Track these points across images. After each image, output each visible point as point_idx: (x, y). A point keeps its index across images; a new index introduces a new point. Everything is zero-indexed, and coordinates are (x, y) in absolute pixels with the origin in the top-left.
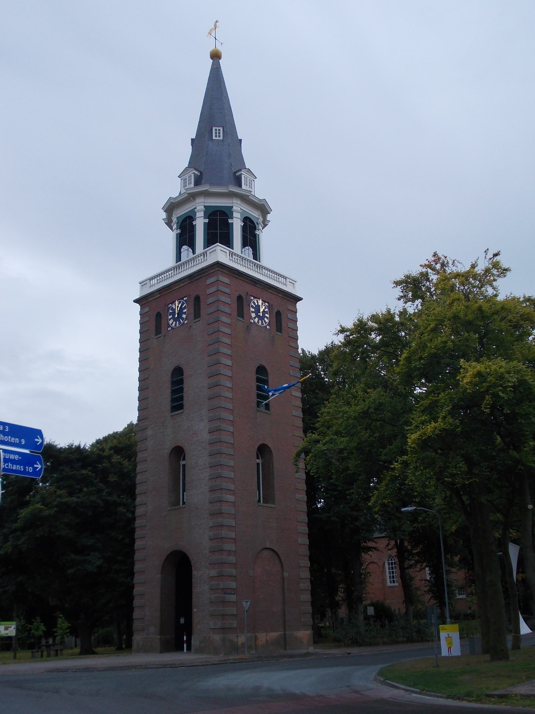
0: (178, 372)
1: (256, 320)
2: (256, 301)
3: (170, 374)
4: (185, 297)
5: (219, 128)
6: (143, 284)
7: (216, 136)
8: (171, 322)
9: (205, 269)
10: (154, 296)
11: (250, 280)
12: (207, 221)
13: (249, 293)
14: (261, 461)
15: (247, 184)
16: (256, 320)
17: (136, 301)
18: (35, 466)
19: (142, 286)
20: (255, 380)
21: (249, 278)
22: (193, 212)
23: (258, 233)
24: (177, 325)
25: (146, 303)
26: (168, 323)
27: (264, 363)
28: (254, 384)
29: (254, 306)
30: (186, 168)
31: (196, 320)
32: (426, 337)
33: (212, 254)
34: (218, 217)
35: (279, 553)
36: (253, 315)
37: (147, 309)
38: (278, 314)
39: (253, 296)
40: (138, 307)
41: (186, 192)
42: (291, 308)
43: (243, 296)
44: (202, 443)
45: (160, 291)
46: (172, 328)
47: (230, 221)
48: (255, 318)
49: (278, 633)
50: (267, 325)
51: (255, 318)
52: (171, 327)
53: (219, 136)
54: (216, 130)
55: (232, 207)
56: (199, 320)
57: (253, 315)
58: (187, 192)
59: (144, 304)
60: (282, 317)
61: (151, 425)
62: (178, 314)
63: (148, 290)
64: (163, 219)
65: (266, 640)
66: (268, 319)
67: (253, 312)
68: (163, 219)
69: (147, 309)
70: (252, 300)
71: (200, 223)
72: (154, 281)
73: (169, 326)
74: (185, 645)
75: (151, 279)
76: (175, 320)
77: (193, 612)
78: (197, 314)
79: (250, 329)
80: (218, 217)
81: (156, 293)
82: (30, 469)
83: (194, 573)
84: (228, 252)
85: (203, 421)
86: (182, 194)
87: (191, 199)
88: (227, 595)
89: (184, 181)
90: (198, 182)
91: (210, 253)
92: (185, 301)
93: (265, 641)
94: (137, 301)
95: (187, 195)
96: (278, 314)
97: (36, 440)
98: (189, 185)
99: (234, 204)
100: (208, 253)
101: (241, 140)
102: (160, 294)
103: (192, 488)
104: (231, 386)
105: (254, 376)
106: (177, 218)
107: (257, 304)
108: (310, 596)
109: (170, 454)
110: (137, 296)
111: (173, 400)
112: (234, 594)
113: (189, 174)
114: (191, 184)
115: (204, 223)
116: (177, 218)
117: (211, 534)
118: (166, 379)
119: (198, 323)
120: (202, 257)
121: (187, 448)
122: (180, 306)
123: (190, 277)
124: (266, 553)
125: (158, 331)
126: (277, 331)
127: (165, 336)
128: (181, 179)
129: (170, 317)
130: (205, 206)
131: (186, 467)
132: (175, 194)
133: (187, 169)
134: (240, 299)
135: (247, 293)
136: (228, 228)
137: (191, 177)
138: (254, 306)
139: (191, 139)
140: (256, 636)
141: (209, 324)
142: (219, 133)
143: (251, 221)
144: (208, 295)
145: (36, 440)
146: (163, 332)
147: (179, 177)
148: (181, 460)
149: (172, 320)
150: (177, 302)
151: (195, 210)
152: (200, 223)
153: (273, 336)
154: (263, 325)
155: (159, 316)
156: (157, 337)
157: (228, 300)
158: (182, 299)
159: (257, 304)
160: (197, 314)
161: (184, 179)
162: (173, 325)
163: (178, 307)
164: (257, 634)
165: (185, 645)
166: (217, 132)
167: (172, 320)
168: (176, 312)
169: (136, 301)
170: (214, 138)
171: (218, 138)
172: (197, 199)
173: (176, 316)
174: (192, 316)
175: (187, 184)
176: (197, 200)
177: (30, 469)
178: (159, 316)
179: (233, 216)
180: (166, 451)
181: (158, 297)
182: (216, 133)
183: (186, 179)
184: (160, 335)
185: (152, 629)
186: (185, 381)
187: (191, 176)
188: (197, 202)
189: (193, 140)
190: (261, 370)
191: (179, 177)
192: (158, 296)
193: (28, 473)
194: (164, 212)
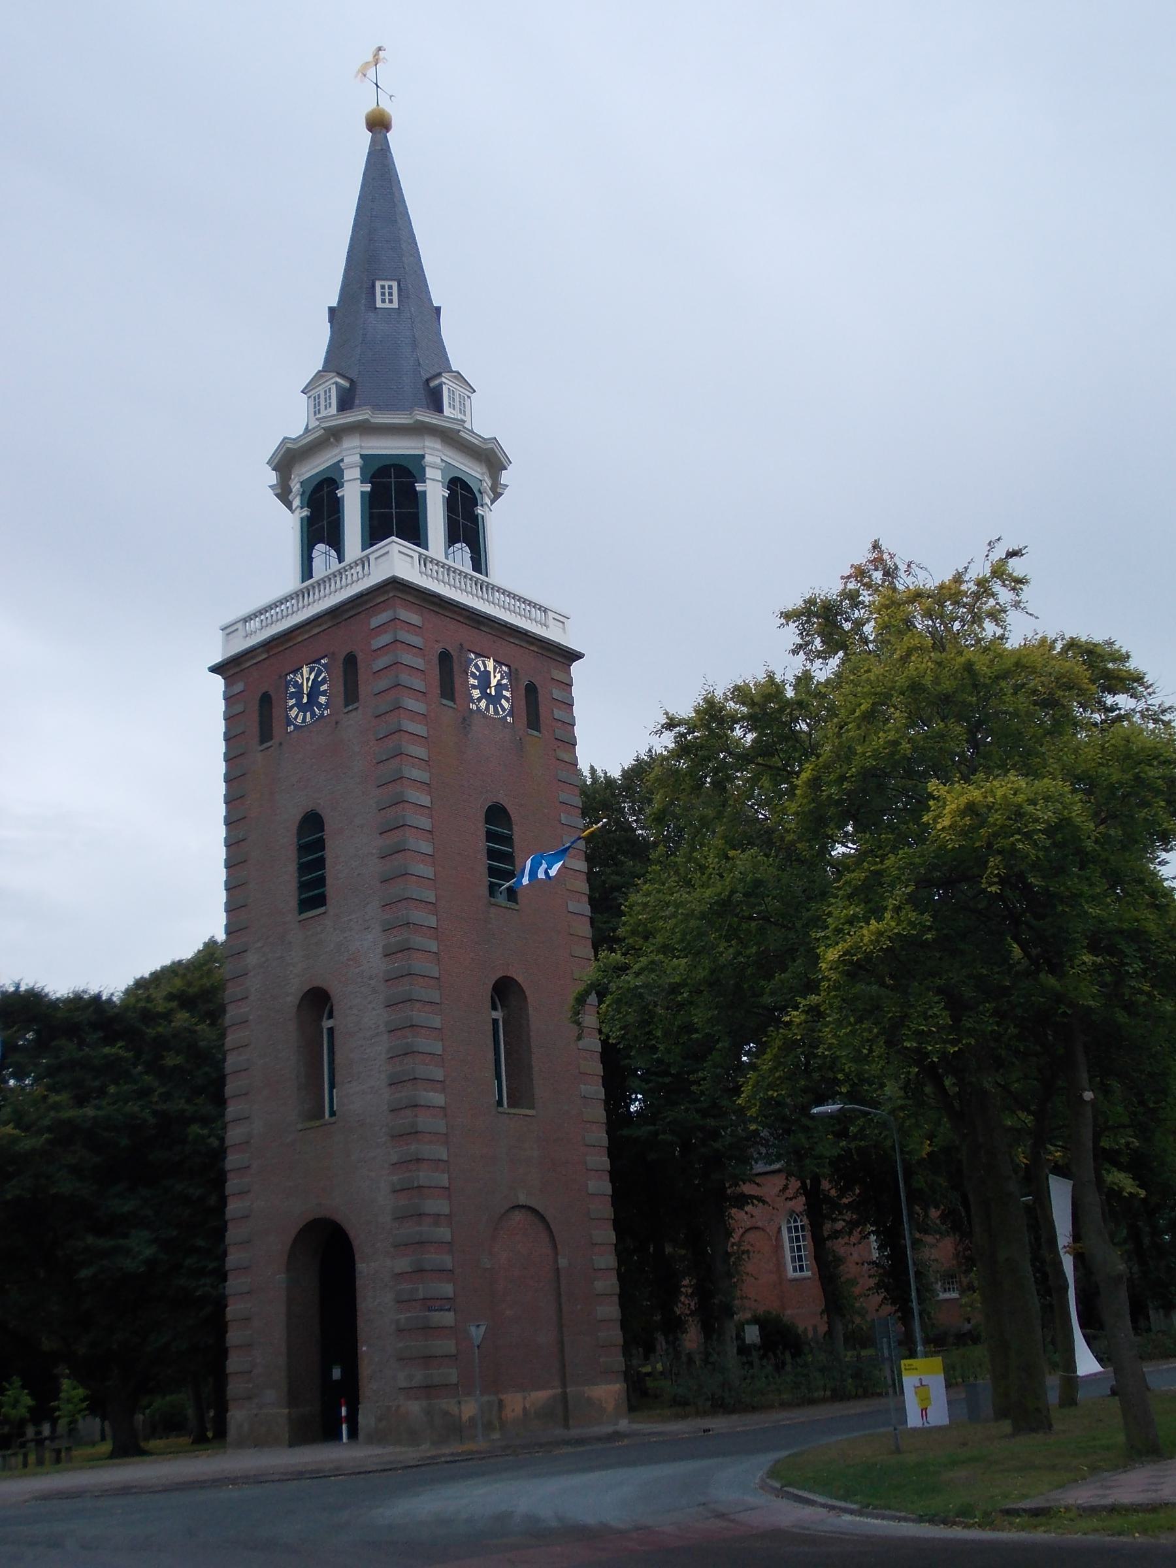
2: (480, 663)
4: (323, 658)
5: (390, 283)
6: (229, 630)
8: (293, 713)
9: (367, 594)
10: (253, 658)
11: (468, 617)
12: (369, 489)
15: (454, 406)
17: (215, 669)
21: (464, 612)
22: (337, 468)
28: (482, 845)
29: (478, 674)
30: (319, 371)
31: (350, 708)
33: (380, 560)
36: (476, 693)
37: (239, 687)
38: (531, 690)
40: (218, 682)
41: (319, 426)
44: (371, 978)
45: (268, 645)
47: (419, 487)
48: (479, 700)
51: (479, 700)
52: (294, 724)
54: (383, 287)
55: (423, 457)
56: (357, 708)
57: (476, 693)
62: (307, 695)
63: (240, 645)
64: (270, 486)
65: (524, 1408)
66: (508, 702)
67: (474, 687)
68: (270, 486)
72: (254, 625)
73: (289, 723)
74: (344, 1427)
76: (302, 707)
78: (351, 695)
79: (469, 725)
80: (393, 480)
84: (416, 556)
85: (370, 929)
87: (332, 440)
90: (346, 402)
91: (376, 558)
95: (322, 431)
96: (531, 690)
99: (427, 451)
100: (372, 558)
101: (438, 309)
102: (268, 652)
103: (349, 1080)
104: (429, 851)
105: (481, 828)
106: (301, 483)
107: (482, 669)
110: (217, 659)
111: (303, 886)
112: (449, 1310)
116: (301, 483)
117: (395, 1178)
118: (286, 841)
119: (354, 713)
120: (359, 568)
122: (312, 677)
123: (334, 613)
124: (518, 1216)
125: (266, 734)
128: (309, 397)
129: (292, 702)
130: (362, 456)
132: (321, 369)
134: (445, 658)
135: (461, 645)
138: (478, 674)
140: (501, 1402)
142: (391, 294)
143: (466, 486)
146: (277, 729)
147: (302, 392)
150: (305, 670)
151: (341, 464)
153: (520, 739)
155: (266, 701)
157: (419, 663)
158: (317, 661)
159: (482, 669)
160: (351, 695)
161: (315, 397)
162: (299, 720)
163: (308, 679)
165: (344, 1427)
168: (305, 692)
169: (215, 669)
170: (379, 304)
171: (387, 305)
172: (344, 442)
173: (305, 700)
174: (340, 700)
175: (322, 397)
178: (266, 701)
180: (289, 999)
182: (383, 294)
183: (319, 395)
187: (330, 388)
189: (332, 310)
190: (497, 814)
191: (302, 392)
192: (264, 656)
194: (273, 470)
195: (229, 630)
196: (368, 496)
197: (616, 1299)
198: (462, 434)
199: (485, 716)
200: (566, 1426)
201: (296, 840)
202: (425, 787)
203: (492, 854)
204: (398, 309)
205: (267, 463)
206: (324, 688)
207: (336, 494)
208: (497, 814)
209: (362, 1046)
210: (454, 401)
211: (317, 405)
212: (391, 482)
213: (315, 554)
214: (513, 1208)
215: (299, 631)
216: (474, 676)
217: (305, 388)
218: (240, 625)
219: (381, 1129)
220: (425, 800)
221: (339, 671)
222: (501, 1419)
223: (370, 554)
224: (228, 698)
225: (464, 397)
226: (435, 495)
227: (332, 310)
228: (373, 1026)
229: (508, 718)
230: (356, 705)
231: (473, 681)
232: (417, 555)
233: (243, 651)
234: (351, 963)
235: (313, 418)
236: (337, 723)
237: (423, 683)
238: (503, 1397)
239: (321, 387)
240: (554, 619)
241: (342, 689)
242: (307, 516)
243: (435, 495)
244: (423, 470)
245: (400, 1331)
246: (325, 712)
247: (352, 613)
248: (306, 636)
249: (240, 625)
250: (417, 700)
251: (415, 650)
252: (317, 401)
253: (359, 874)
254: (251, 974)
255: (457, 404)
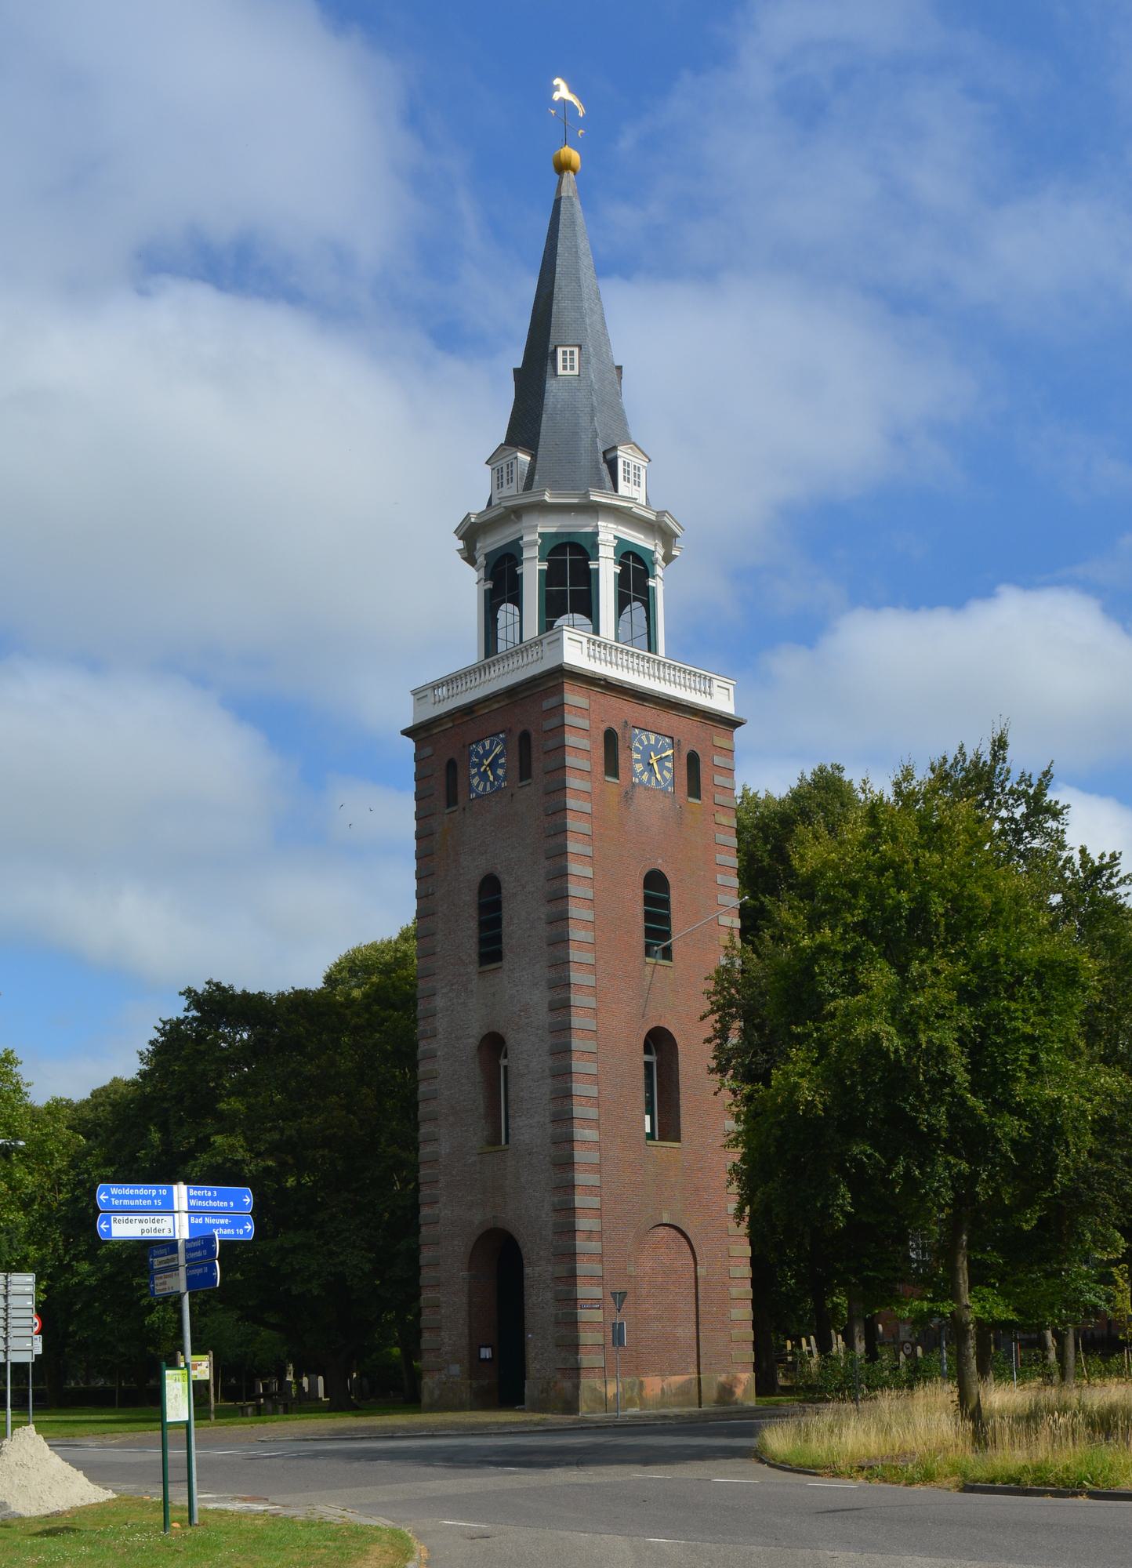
0: (490, 886)
1: (645, 777)
2: (644, 738)
3: (475, 887)
5: (572, 349)
6: (419, 694)
7: (565, 368)
9: (539, 679)
10: (441, 725)
12: (546, 567)
13: (629, 722)
14: (656, 1058)
15: (628, 478)
16: (645, 777)
17: (407, 733)
18: (246, 1227)
19: (418, 699)
20: (641, 902)
23: (654, 585)
24: (488, 789)
25: (427, 737)
26: (470, 784)
27: (660, 864)
28: (639, 909)
29: (641, 748)
30: (502, 444)
31: (524, 783)
32: (987, 803)
34: (568, 557)
35: (689, 1235)
36: (639, 767)
37: (428, 751)
38: (693, 760)
39: (637, 728)
40: (410, 744)
41: (500, 504)
42: (719, 742)
43: (616, 730)
45: (451, 715)
46: (479, 796)
47: (592, 565)
48: (642, 773)
49: (686, 1377)
50: (667, 786)
51: (642, 773)
52: (476, 792)
53: (572, 368)
54: (565, 353)
55: (596, 534)
56: (530, 784)
57: (639, 767)
58: (504, 504)
59: (423, 739)
60: (702, 766)
61: (442, 988)
63: (432, 711)
64: (458, 550)
65: (662, 1389)
66: (669, 772)
67: (637, 761)
68: (458, 550)
69: (428, 751)
70: (636, 735)
71: (532, 571)
72: (442, 692)
73: (471, 789)
75: (435, 686)
77: (526, 1339)
78: (525, 772)
79: (631, 798)
81: (445, 720)
82: (241, 1232)
83: (528, 1270)
84: (585, 640)
86: (495, 506)
87: (513, 517)
88: (584, 1310)
89: (498, 473)
91: (548, 644)
92: (501, 740)
93: (660, 1392)
94: (410, 732)
95: (502, 510)
97: (245, 1200)
98: (508, 483)
100: (545, 642)
101: (619, 368)
102: (453, 721)
103: (520, 1114)
104: (591, 918)
105: (640, 893)
106: (485, 555)
107: (646, 743)
108: (750, 1309)
109: (480, 1048)
110: (409, 723)
111: (482, 942)
112: (598, 1308)
113: (508, 459)
114: (512, 482)
115: (615, 573)
116: (485, 555)
117: (556, 1199)
118: (469, 899)
119: (528, 788)
121: (511, 1038)
123: (512, 692)
124: (663, 1232)
125: (452, 799)
126: (690, 794)
127: (464, 809)
128: (493, 469)
129: (474, 771)
131: (509, 1069)
132: (476, 504)
133: (505, 449)
134: (610, 737)
135: (626, 722)
136: (588, 579)
137: (512, 467)
138: (641, 748)
139: (514, 369)
140: (641, 1383)
141: (548, 794)
142: (572, 360)
143: (638, 559)
144: (545, 732)
145: (245, 1200)
146: (461, 798)
147: (487, 463)
148: (502, 1057)
149: (477, 777)
152: (532, 571)
153: (680, 807)
154: (661, 785)
155: (451, 766)
156: (450, 810)
157: (584, 743)
158: (496, 735)
159: (646, 743)
161: (498, 470)
162: (480, 788)
164: (643, 1379)
166: (566, 359)
167: (477, 777)
169: (407, 733)
170: (560, 371)
171: (568, 372)
172: (523, 519)
174: (515, 774)
175: (505, 470)
176: (524, 521)
177: (241, 1232)
178: (451, 766)
179: (598, 553)
180: (471, 1040)
181: (451, 727)
182: (565, 360)
184: (454, 808)
185: (455, 1369)
186: (504, 905)
187: (512, 463)
188: (524, 525)
189: (516, 371)
190: (655, 882)
191: (487, 463)
192: (451, 725)
193: (240, 1236)
194: (460, 539)
195: (419, 694)
196: (545, 573)
197: (749, 1303)
198: (634, 510)
199: (647, 789)
200: (700, 1407)
201: (477, 899)
202: (589, 903)
203: (648, 917)
204: (579, 376)
205: (455, 532)
206: (502, 761)
207: (516, 571)
208: (655, 882)
209: (530, 1087)
210: (629, 474)
211: (500, 478)
212: (570, 555)
213: (501, 615)
214: (657, 1226)
215: (480, 706)
216: (637, 751)
217: (489, 460)
218: (429, 692)
219: (544, 1158)
220: (588, 872)
221: (514, 742)
222: (641, 1394)
223: (543, 639)
224: (418, 759)
225: (639, 468)
226: (607, 570)
227: (516, 371)
228: (540, 1070)
229: (669, 788)
230: (529, 781)
231: (636, 756)
232: (586, 639)
233: (434, 718)
234: (522, 1013)
235: (496, 492)
236: (512, 795)
237: (589, 763)
238: (643, 1379)
239: (505, 460)
240: (718, 686)
241: (517, 764)
242: (490, 589)
243: (607, 570)
244: (596, 546)
245: (557, 1323)
246: (503, 784)
247: (528, 693)
248: (486, 711)
249: (429, 692)
250: (582, 779)
251: (582, 732)
252: (500, 474)
253: (529, 936)
254: (440, 1015)
255: (632, 477)
